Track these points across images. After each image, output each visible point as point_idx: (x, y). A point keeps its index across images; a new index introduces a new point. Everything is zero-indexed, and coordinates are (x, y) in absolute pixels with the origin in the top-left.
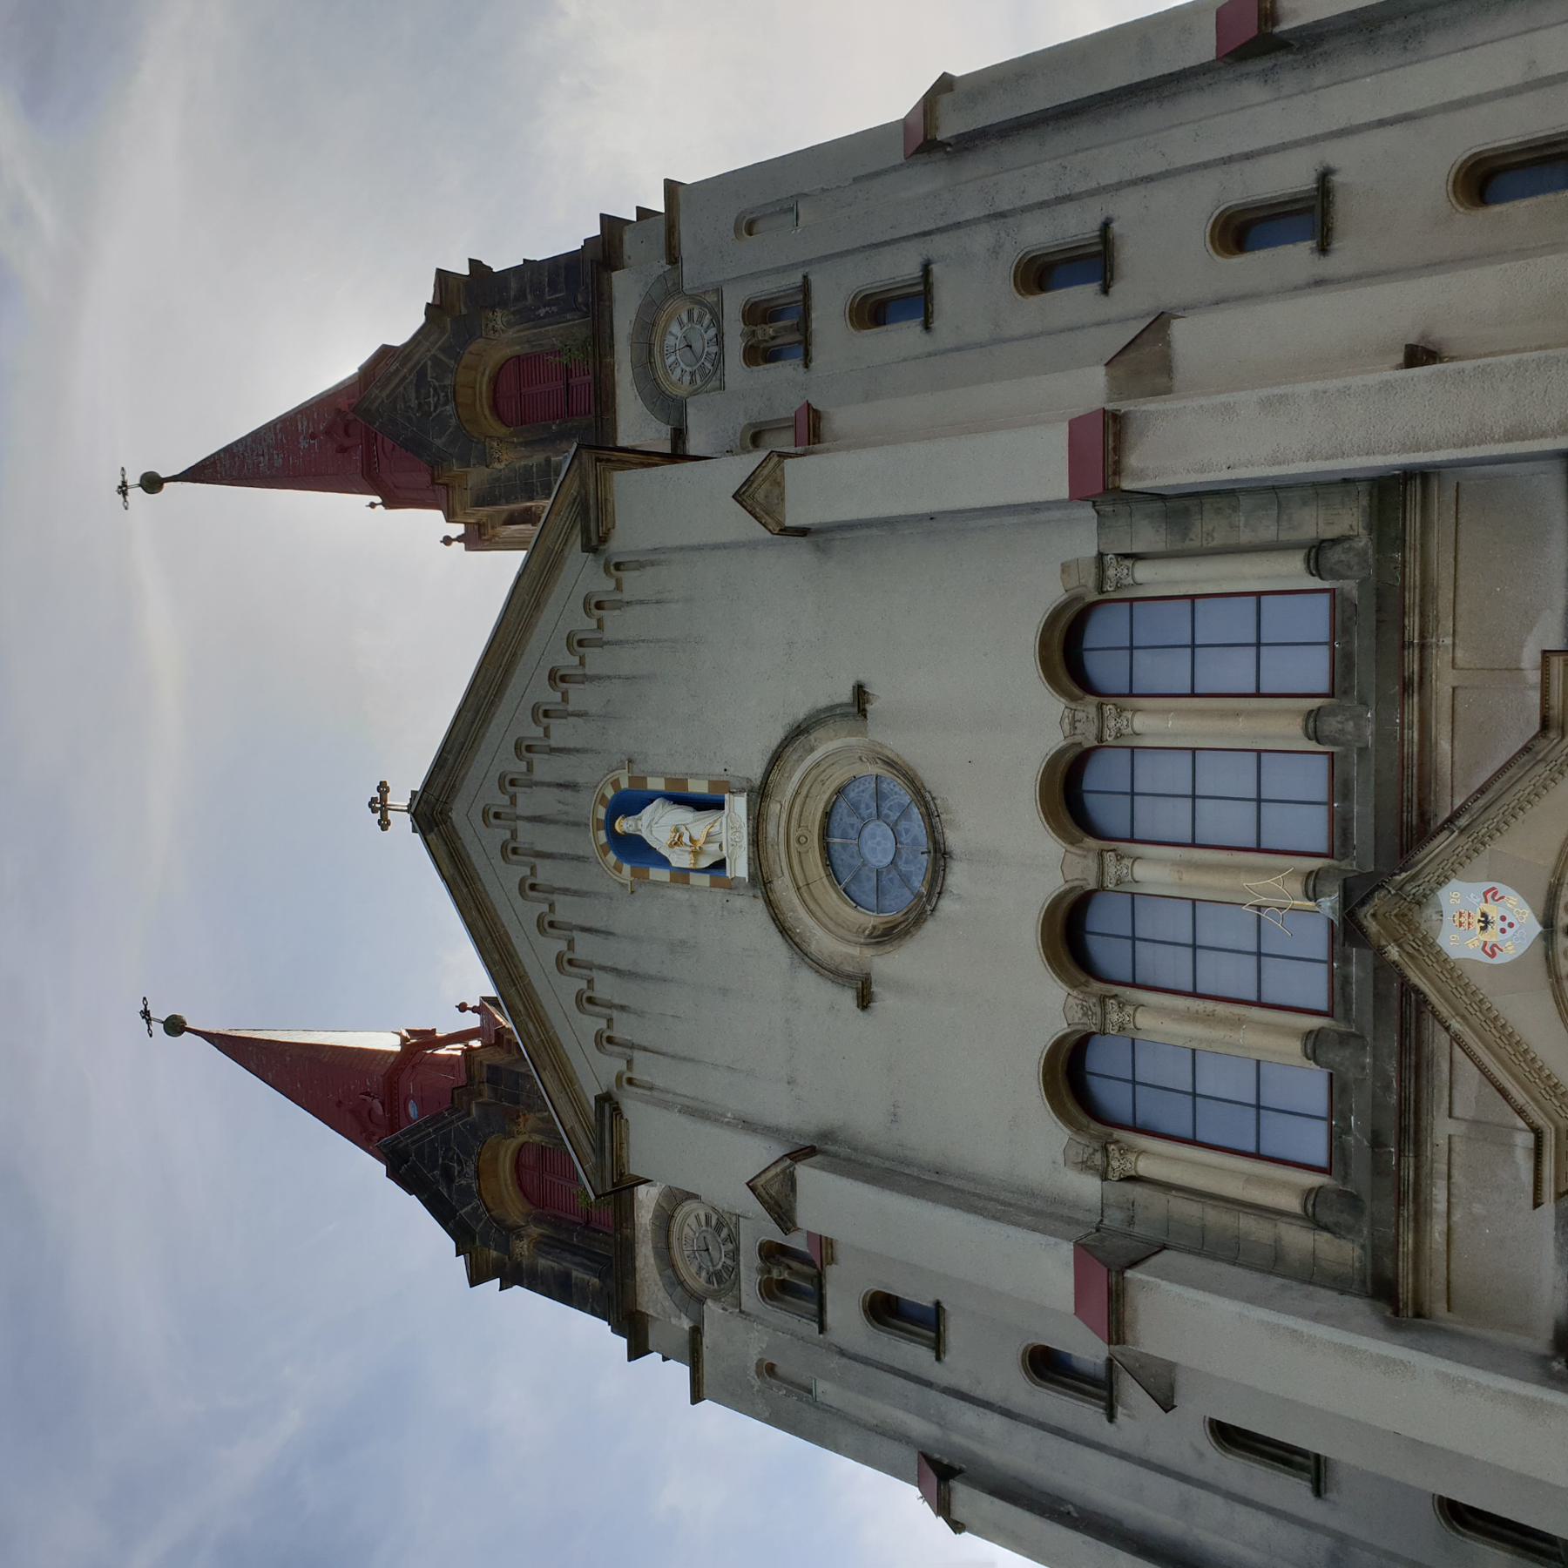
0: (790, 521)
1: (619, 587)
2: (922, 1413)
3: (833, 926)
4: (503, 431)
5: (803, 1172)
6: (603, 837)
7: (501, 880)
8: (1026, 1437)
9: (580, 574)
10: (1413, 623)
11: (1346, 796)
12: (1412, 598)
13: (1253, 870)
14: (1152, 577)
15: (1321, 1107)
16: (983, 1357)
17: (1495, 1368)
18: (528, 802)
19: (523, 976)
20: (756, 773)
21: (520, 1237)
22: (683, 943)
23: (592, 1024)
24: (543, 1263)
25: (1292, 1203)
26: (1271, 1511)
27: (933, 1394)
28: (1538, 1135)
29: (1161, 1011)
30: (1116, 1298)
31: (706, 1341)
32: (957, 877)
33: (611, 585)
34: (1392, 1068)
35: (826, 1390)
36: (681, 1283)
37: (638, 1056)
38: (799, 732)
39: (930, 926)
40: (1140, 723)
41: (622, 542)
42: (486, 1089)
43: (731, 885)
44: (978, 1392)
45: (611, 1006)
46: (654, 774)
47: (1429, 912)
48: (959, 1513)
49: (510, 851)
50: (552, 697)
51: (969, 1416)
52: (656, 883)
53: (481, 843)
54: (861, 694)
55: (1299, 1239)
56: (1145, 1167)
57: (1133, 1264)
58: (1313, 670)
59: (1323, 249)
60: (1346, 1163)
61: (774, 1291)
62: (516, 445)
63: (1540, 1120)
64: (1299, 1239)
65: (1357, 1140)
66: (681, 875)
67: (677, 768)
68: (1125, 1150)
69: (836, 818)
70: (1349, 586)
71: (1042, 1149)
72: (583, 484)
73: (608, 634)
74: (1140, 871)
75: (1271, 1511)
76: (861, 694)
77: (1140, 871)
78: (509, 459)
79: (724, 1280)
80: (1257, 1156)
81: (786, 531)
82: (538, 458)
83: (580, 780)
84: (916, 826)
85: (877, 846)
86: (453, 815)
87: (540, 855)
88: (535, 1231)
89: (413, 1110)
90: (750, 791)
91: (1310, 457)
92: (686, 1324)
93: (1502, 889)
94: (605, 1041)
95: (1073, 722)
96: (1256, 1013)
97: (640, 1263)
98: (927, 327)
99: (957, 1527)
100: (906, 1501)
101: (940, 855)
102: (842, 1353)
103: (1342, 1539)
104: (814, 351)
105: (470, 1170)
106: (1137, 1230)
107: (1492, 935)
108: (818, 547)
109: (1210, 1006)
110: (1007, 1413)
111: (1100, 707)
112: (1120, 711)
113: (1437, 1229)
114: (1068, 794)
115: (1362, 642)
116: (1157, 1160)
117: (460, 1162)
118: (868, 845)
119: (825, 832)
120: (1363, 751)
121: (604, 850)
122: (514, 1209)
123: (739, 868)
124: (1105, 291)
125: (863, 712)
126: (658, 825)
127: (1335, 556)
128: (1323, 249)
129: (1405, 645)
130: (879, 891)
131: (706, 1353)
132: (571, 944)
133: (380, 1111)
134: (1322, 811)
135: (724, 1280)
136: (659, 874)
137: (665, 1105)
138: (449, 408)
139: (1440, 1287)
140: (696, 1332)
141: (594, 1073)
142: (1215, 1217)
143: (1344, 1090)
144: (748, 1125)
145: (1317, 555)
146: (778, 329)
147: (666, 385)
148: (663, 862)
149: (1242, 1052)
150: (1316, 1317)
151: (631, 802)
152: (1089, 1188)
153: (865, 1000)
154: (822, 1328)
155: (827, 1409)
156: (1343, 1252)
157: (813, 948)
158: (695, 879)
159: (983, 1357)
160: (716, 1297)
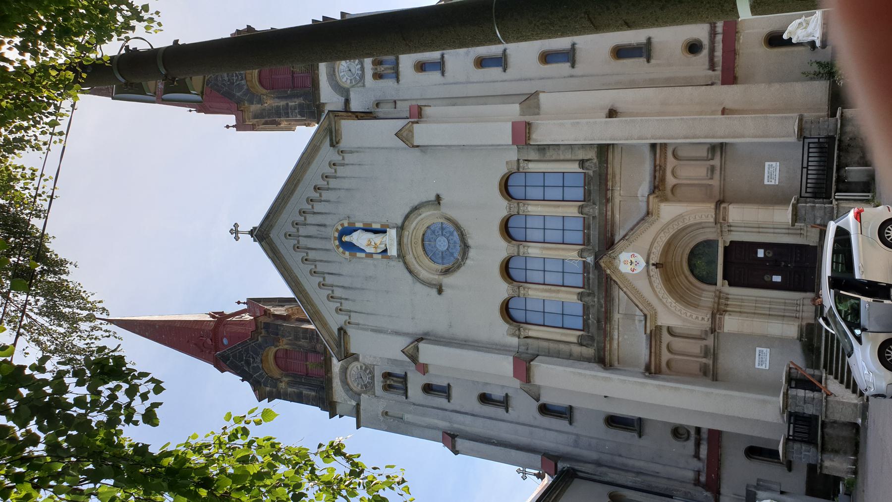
0: (415, 144)
1: (343, 159)
2: (443, 419)
3: (427, 269)
4: (264, 91)
5: (422, 345)
6: (337, 243)
7: (294, 259)
8: (480, 422)
9: (327, 153)
10: (610, 184)
11: (589, 228)
12: (610, 177)
13: (563, 249)
14: (533, 167)
15: (581, 313)
16: (464, 398)
17: (633, 376)
18: (303, 231)
19: (304, 290)
20: (399, 222)
21: (281, 382)
22: (370, 277)
23: (334, 305)
24: (290, 390)
25: (574, 340)
26: (557, 431)
27: (447, 413)
28: (645, 316)
29: (536, 289)
30: (528, 370)
31: (361, 408)
32: (472, 253)
33: (341, 158)
34: (602, 301)
35: (408, 417)
36: (351, 390)
37: (352, 314)
38: (415, 209)
39: (463, 268)
40: (530, 208)
41: (344, 144)
42: (263, 331)
43: (389, 258)
44: (463, 410)
45: (341, 298)
46: (359, 222)
47: (617, 261)
48: (458, 448)
49: (297, 248)
50: (315, 195)
51: (460, 417)
52: (360, 258)
53: (285, 247)
54: (438, 198)
55: (577, 349)
56: (531, 334)
57: (532, 360)
58: (579, 193)
59: (573, 66)
60: (589, 328)
61: (387, 388)
62: (274, 98)
63: (646, 312)
64: (577, 349)
65: (592, 320)
66: (370, 255)
67: (368, 220)
68: (525, 329)
69: (426, 235)
70: (591, 173)
71: (501, 331)
72: (330, 124)
73: (338, 175)
74: (530, 250)
75: (557, 431)
76: (438, 198)
77: (530, 250)
78: (271, 102)
79: (368, 387)
80: (563, 328)
81: (414, 146)
82: (282, 103)
83: (327, 223)
84: (456, 237)
85: (442, 244)
86: (271, 235)
87: (309, 249)
88: (286, 379)
89: (225, 341)
90: (397, 228)
91: (585, 140)
92: (354, 403)
93: (636, 254)
94: (339, 310)
95: (510, 208)
96: (563, 288)
97: (334, 385)
98: (443, 74)
99: (456, 452)
100: (439, 449)
101: (466, 247)
102: (414, 404)
103: (577, 435)
104: (400, 78)
105: (258, 360)
106: (529, 351)
107: (633, 266)
108: (422, 151)
109: (549, 287)
110: (473, 415)
111: (518, 204)
112: (524, 205)
113: (615, 343)
114: (506, 229)
115: (594, 188)
116: (534, 331)
117: (253, 358)
118: (438, 243)
119: (423, 240)
120: (594, 218)
121: (338, 247)
122: (276, 373)
123: (393, 251)
124: (505, 71)
125: (439, 203)
126: (359, 239)
127: (587, 164)
128: (573, 66)
129: (607, 190)
130: (443, 258)
131: (362, 411)
132: (324, 279)
133: (210, 342)
134: (581, 233)
135: (368, 387)
136: (359, 255)
137: (366, 330)
138: (243, 82)
139: (616, 358)
140: (358, 405)
141: (335, 321)
142: (552, 345)
143: (588, 308)
144: (397, 333)
145: (582, 163)
146: (719, 298)
147: (342, 84)
148: (363, 251)
149: (557, 298)
150: (585, 369)
151: (350, 230)
152: (515, 341)
153: (440, 291)
154: (407, 398)
155: (409, 423)
156: (589, 351)
157: (421, 277)
158: (375, 256)
159: (464, 398)
160: (365, 393)
